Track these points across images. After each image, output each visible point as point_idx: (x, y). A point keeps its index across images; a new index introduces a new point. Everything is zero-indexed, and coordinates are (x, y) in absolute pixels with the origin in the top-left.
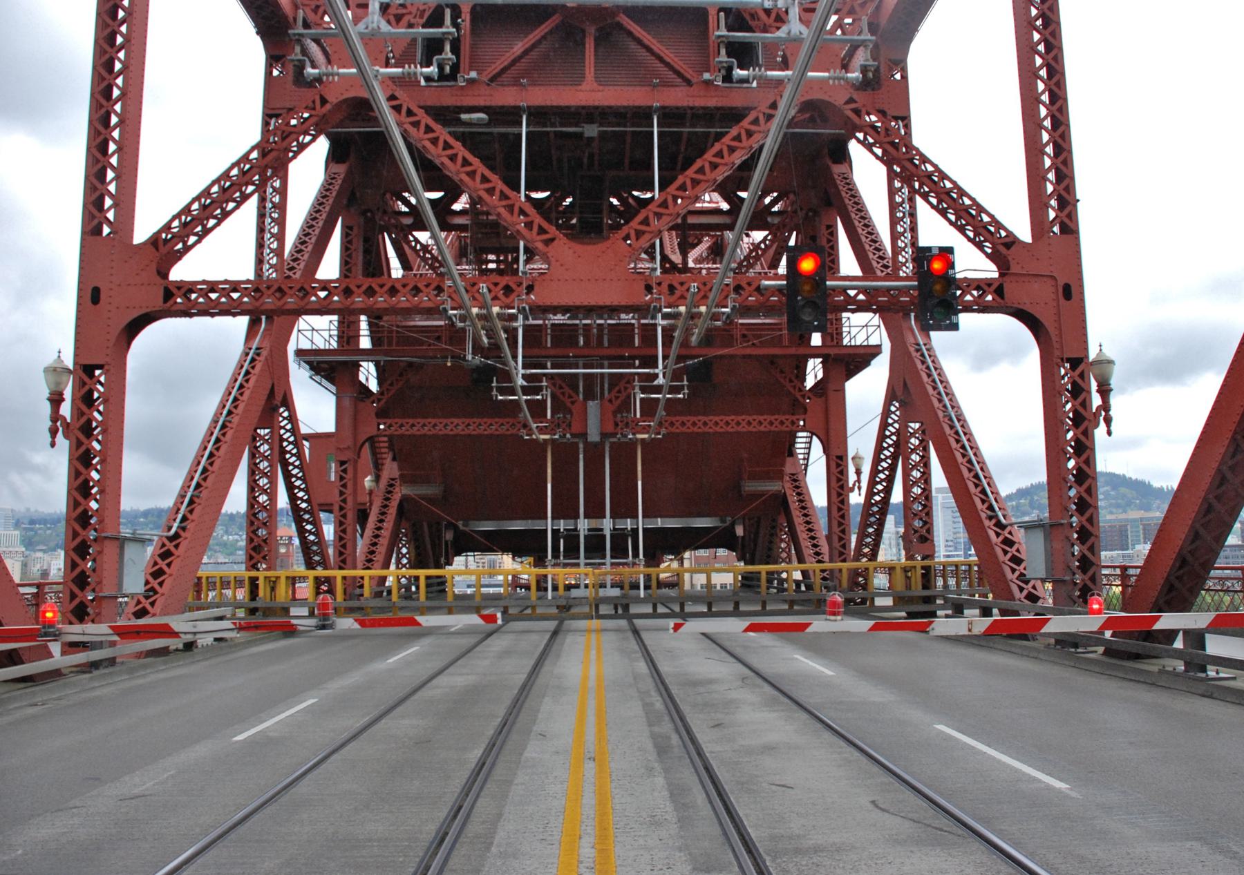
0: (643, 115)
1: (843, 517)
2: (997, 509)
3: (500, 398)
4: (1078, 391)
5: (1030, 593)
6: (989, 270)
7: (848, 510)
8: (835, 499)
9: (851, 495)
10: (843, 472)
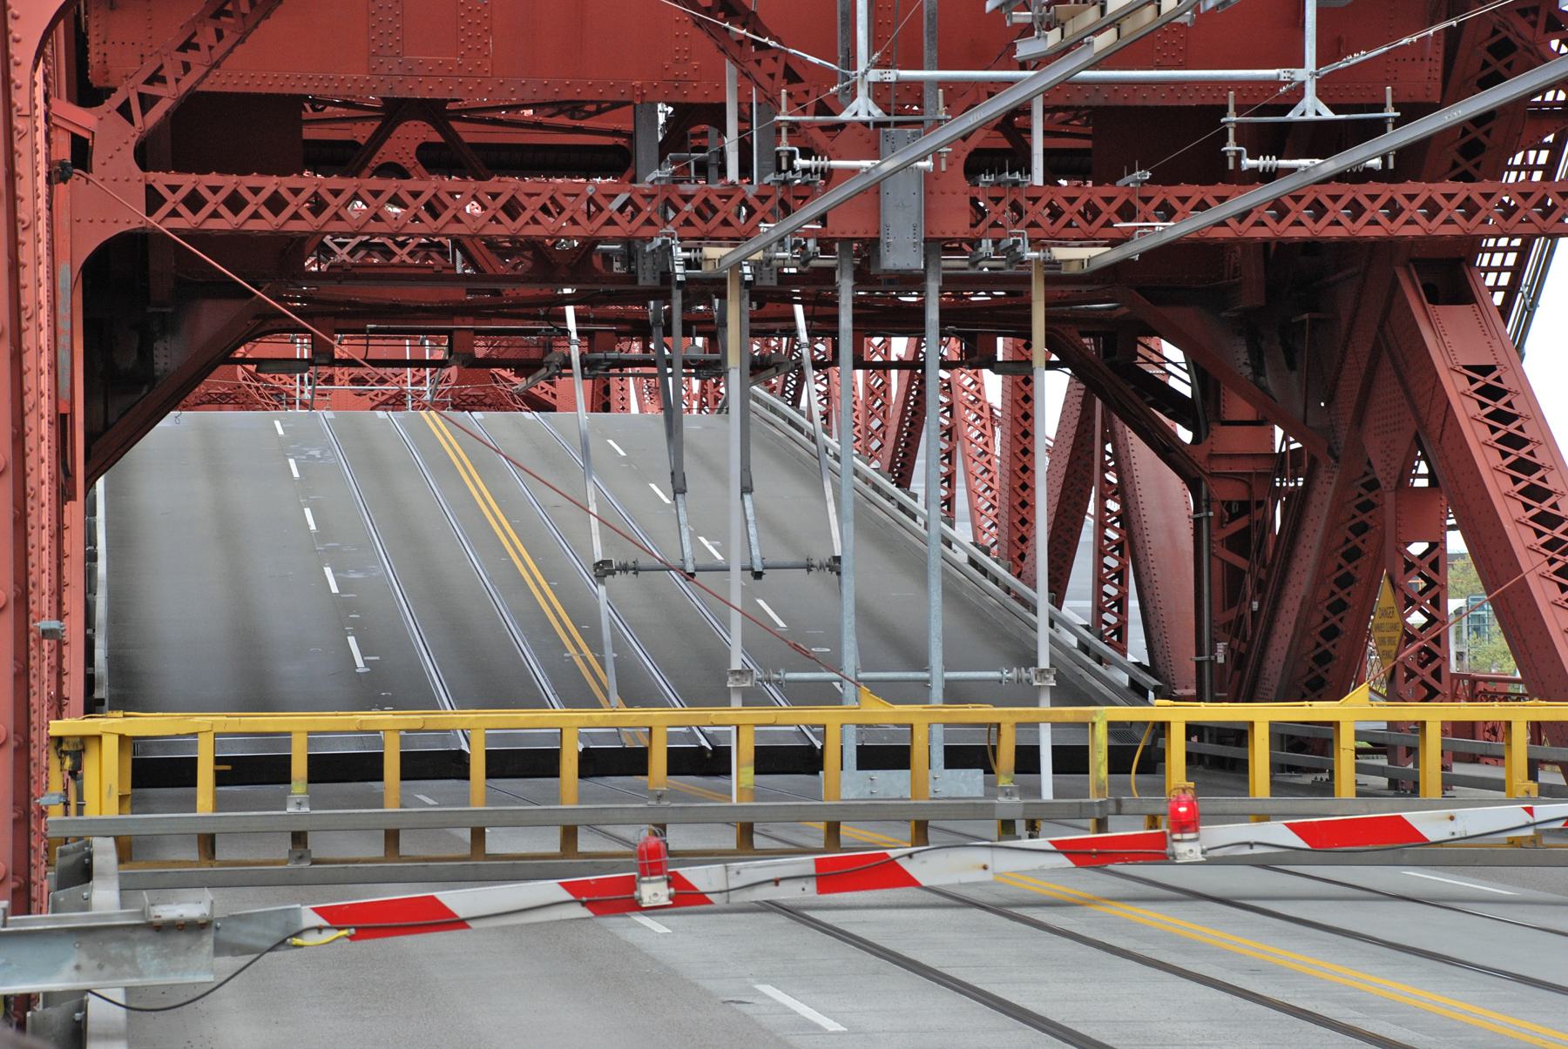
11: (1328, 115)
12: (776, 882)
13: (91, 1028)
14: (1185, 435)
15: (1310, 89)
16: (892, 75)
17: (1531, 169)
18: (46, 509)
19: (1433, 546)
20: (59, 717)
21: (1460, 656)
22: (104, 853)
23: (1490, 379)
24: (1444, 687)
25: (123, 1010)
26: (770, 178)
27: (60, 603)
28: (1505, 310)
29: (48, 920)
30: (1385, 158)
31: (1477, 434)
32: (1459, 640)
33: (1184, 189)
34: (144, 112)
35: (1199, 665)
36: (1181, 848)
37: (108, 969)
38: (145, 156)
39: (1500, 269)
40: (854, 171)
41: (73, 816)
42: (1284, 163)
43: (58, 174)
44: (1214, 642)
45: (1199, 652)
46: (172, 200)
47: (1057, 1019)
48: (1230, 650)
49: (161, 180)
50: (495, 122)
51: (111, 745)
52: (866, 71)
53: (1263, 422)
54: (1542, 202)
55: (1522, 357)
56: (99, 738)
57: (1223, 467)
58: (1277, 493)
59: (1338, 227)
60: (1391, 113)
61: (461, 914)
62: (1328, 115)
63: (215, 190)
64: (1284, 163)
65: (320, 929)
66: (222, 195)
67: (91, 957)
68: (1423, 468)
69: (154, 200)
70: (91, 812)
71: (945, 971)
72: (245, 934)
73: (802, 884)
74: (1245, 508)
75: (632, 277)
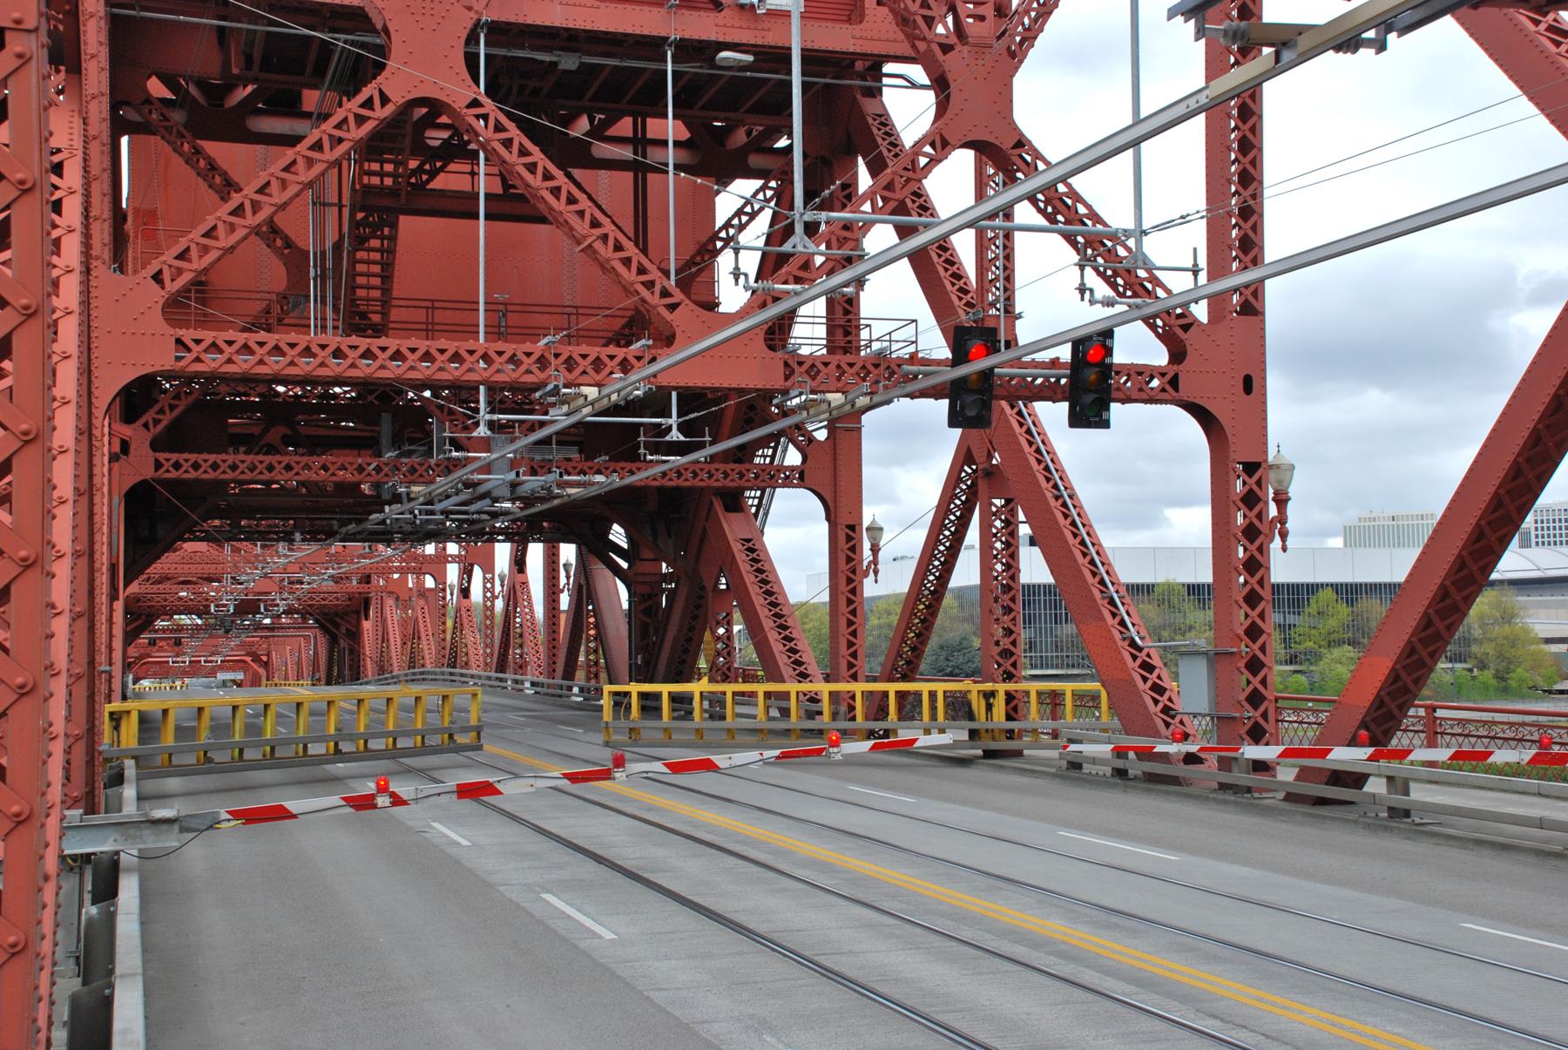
0: (652, 46)
1: (853, 613)
2: (1062, 488)
3: (454, 454)
4: (1251, 500)
5: (1154, 683)
6: (1159, 356)
7: (861, 603)
8: (843, 587)
9: (865, 580)
10: (855, 549)
11: (682, 438)
12: (439, 795)
13: (122, 865)
14: (625, 565)
15: (675, 427)
16: (495, 417)
17: (765, 457)
18: (104, 576)
19: (728, 614)
20: (110, 702)
21: (740, 649)
22: (129, 764)
23: (750, 545)
24: (732, 675)
25: (136, 859)
26: (441, 457)
27: (110, 658)
28: (756, 515)
29: (103, 819)
30: (706, 458)
31: (745, 568)
32: (740, 643)
33: (623, 464)
34: (155, 427)
35: (630, 665)
36: (617, 775)
37: (130, 841)
38: (156, 446)
39: (754, 498)
40: (479, 458)
41: (115, 748)
42: (664, 458)
43: (114, 458)
44: (637, 654)
45: (630, 660)
46: (167, 465)
47: (564, 836)
48: (643, 658)
49: (162, 456)
50: (316, 426)
51: (135, 717)
52: (484, 415)
53: (658, 560)
54: (769, 474)
55: (763, 534)
56: (128, 712)
57: (641, 579)
58: (663, 590)
59: (687, 482)
60: (708, 439)
61: (295, 812)
62: (682, 438)
63: (187, 461)
64: (664, 458)
65: (229, 820)
66: (190, 463)
67: (122, 836)
68: (724, 581)
69: (158, 465)
70: (124, 745)
71: (516, 814)
72: (193, 824)
73: (449, 796)
74: (650, 597)
75: (379, 496)
